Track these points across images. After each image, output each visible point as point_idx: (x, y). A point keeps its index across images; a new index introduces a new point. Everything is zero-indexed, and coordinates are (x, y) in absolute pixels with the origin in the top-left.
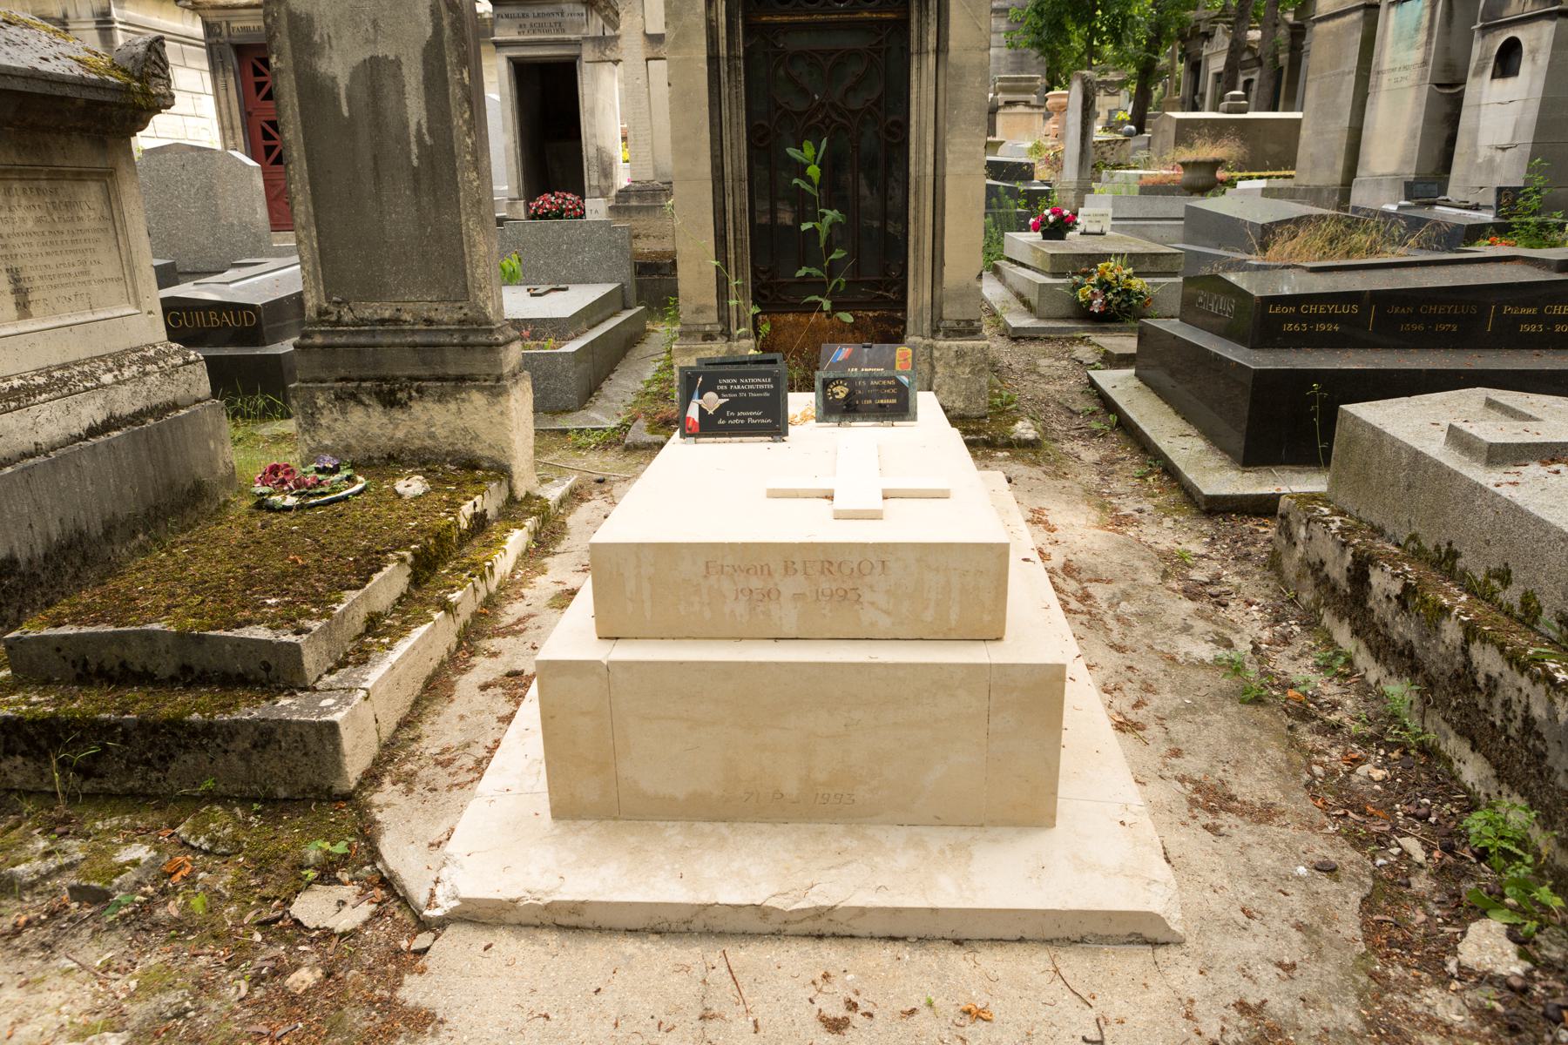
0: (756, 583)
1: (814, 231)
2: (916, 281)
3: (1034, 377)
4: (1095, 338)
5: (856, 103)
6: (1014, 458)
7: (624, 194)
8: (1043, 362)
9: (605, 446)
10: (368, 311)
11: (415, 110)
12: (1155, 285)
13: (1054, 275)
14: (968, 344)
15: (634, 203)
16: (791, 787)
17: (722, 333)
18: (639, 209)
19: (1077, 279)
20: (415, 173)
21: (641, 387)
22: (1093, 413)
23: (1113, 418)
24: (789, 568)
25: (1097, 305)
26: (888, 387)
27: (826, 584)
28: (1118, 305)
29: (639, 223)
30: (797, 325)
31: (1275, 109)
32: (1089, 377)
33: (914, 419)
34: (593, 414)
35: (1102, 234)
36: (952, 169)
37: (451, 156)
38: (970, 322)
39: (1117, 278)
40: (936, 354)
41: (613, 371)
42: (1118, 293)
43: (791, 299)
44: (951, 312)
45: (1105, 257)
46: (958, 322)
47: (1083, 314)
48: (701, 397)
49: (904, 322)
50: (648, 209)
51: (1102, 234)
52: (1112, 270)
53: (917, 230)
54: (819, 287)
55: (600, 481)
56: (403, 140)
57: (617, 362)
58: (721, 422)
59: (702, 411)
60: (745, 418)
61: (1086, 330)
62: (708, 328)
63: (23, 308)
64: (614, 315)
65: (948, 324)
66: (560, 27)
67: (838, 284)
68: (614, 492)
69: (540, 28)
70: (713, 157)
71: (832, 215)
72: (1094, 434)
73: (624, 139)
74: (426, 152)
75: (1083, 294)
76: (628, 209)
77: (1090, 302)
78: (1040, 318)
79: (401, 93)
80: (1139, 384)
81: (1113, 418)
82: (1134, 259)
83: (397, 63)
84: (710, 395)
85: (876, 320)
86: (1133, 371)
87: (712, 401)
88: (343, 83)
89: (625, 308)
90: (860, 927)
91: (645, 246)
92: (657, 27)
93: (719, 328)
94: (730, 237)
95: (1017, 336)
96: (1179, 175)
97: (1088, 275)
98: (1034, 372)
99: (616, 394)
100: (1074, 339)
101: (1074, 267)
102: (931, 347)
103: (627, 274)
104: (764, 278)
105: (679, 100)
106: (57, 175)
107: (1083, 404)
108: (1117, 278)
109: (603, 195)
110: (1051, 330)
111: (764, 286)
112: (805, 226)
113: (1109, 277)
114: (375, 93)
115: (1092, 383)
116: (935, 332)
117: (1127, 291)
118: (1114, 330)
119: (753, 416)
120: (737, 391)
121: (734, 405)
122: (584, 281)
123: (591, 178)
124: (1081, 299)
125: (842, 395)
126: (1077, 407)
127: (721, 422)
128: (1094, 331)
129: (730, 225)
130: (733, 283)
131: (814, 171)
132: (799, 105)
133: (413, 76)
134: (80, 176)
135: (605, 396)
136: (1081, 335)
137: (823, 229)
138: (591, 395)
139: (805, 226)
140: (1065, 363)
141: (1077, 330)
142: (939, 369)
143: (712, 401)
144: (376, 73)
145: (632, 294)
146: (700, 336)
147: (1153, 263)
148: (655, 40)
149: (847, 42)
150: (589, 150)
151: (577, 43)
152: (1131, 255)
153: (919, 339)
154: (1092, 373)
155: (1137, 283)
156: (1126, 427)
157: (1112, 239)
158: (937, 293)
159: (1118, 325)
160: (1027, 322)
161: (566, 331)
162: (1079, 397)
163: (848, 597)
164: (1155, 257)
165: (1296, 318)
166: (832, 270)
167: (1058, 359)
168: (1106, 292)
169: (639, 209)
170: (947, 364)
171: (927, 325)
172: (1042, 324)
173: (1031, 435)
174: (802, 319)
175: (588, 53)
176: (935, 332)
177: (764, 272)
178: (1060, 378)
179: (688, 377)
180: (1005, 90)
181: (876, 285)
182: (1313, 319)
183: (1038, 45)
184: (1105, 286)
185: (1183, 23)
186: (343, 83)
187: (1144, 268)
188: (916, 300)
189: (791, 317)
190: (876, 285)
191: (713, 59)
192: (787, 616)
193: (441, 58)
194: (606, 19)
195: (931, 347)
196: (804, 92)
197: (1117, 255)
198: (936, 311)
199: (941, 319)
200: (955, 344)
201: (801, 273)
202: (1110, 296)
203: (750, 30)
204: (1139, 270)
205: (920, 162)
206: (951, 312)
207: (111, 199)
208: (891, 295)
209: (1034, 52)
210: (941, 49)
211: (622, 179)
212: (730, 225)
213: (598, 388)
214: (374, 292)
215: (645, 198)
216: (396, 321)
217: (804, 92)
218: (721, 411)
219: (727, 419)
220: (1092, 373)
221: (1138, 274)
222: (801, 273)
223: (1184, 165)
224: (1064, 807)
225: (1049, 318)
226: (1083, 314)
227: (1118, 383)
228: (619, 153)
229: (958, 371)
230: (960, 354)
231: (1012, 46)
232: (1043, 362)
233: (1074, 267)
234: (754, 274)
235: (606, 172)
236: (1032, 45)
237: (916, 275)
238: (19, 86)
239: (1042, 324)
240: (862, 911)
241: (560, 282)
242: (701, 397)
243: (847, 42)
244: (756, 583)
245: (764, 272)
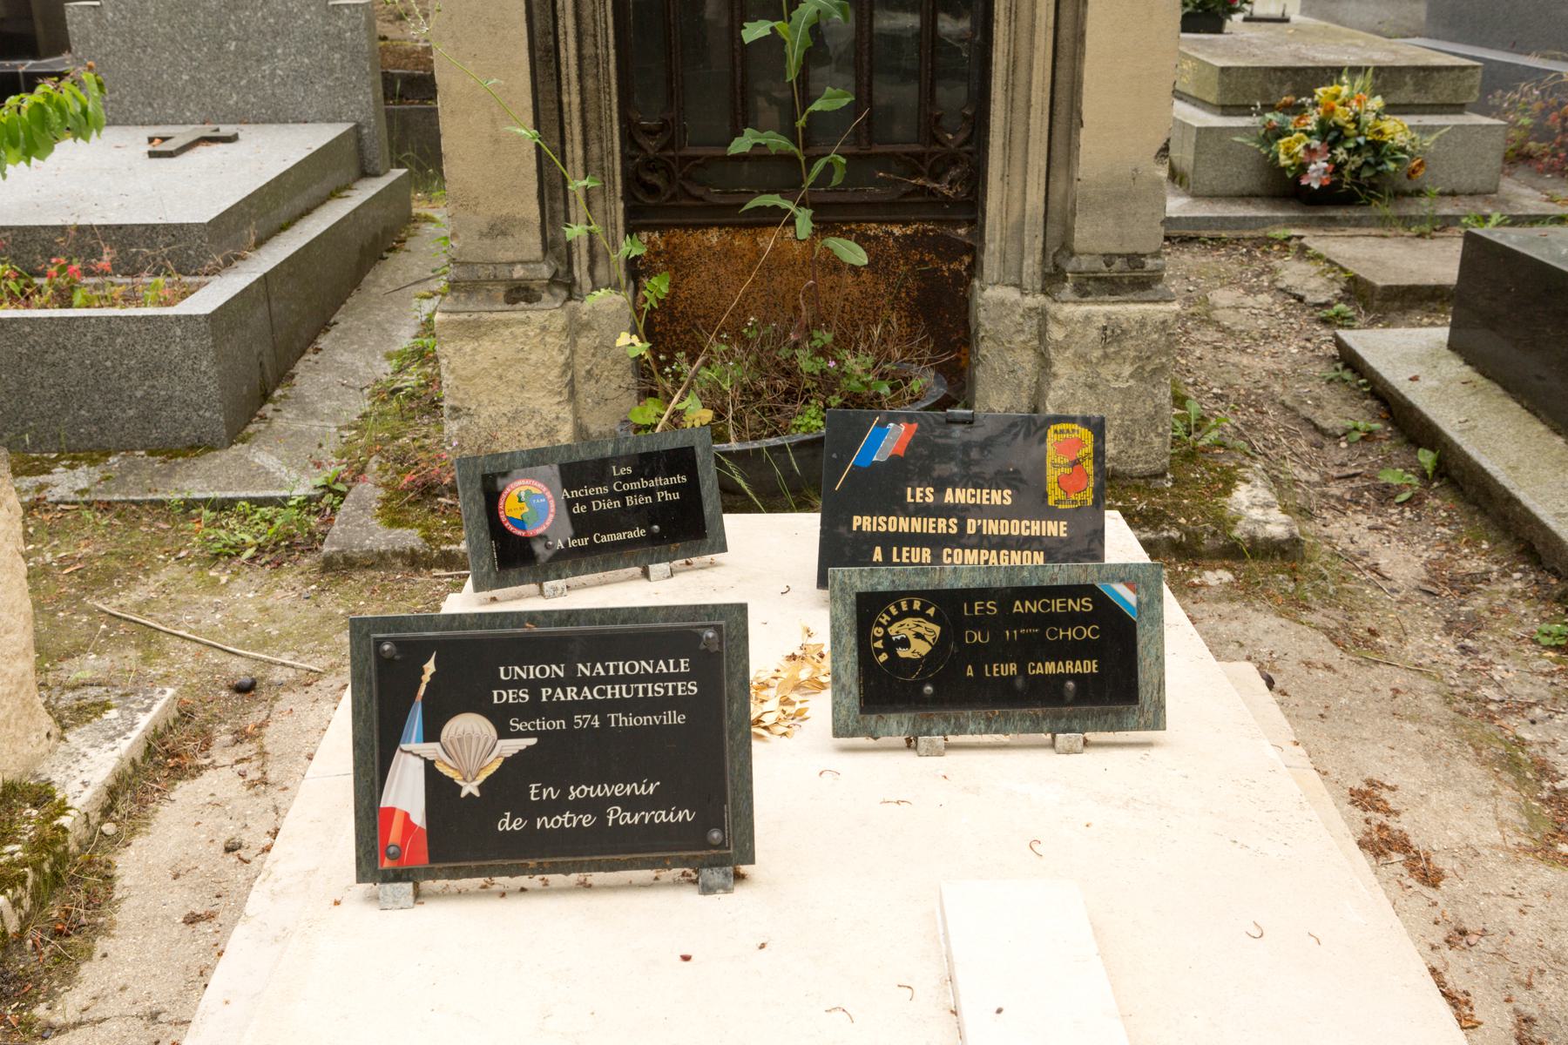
1: (773, 42)
2: (1008, 160)
3: (1211, 334)
4: (1316, 241)
6: (1246, 590)
8: (1223, 297)
9: (280, 551)
12: (1426, 130)
13: (1226, 110)
14: (1129, 310)
17: (553, 281)
19: (1274, 118)
21: (384, 369)
22: (1369, 436)
23: (1426, 458)
25: (1316, 174)
26: (1071, 619)
28: (1356, 173)
30: (728, 253)
32: (1339, 344)
33: (1157, 721)
34: (263, 457)
35: (1284, 20)
38: (1134, 259)
39: (1356, 120)
40: (1056, 333)
41: (325, 326)
42: (1357, 149)
43: (714, 196)
44: (1094, 236)
45: (1330, 74)
46: (1109, 258)
47: (1285, 188)
48: (432, 733)
49: (973, 250)
51: (1284, 20)
52: (1348, 100)
53: (1013, 39)
54: (780, 171)
55: (245, 689)
57: (338, 301)
58: (509, 824)
59: (438, 786)
60: (597, 806)
61: (1290, 222)
62: (519, 272)
64: (335, 193)
65: (1085, 264)
67: (829, 168)
68: (271, 734)
70: (1079, 37)
72: (1386, 495)
75: (1288, 150)
77: (1303, 168)
78: (1195, 196)
80: (1467, 371)
81: (1426, 458)
82: (1386, 78)
84: (468, 727)
85: (908, 243)
86: (1442, 333)
87: (474, 747)
89: (365, 173)
93: (545, 271)
94: (569, 52)
98: (1207, 321)
99: (326, 394)
100: (1269, 241)
101: (1266, 94)
102: (1043, 314)
103: (365, 100)
104: (651, 145)
107: (1343, 413)
108: (1356, 120)
110: (1224, 222)
111: (651, 165)
112: (754, 31)
113: (1342, 116)
115: (1350, 360)
116: (1052, 278)
117: (1376, 146)
118: (1347, 222)
119: (623, 799)
120: (565, 710)
122: (276, 114)
124: (1284, 161)
125: (920, 648)
126: (1331, 422)
127: (509, 824)
128: (1305, 224)
129: (568, 22)
130: (577, 184)
135: (300, 400)
136: (1281, 233)
138: (265, 397)
139: (754, 31)
140: (1265, 299)
141: (1274, 222)
142: (1062, 368)
145: (378, 143)
146: (500, 291)
147: (1420, 87)
152: (1379, 70)
153: (1012, 294)
154: (1346, 335)
155: (1397, 129)
156: (1459, 478)
157: (1300, 31)
158: (1059, 186)
159: (1355, 213)
161: (203, 255)
162: (1324, 391)
164: (1425, 74)
166: (815, 134)
167: (1250, 291)
168: (1333, 145)
170: (1082, 358)
171: (1032, 265)
172: (1203, 210)
173: (1277, 525)
174: (741, 241)
176: (1052, 278)
177: (650, 133)
178: (1265, 336)
179: (383, 663)
181: (913, 164)
184: (1331, 134)
187: (1402, 97)
188: (1006, 204)
189: (713, 237)
190: (913, 164)
195: (1043, 314)
197: (1355, 70)
198: (1055, 231)
199: (1067, 248)
200: (1101, 310)
201: (742, 145)
202: (1341, 154)
204: (1393, 99)
206: (1094, 236)
208: (943, 188)
212: (568, 22)
213: (284, 375)
218: (507, 783)
219: (530, 811)
220: (1346, 335)
221: (1392, 109)
222: (742, 145)
225: (1213, 197)
226: (1285, 188)
227: (1412, 355)
229: (1106, 372)
230: (1112, 335)
232: (1223, 297)
233: (1266, 94)
234: (628, 138)
237: (1008, 144)
239: (1203, 210)
241: (225, 120)
242: (432, 733)
245: (650, 133)
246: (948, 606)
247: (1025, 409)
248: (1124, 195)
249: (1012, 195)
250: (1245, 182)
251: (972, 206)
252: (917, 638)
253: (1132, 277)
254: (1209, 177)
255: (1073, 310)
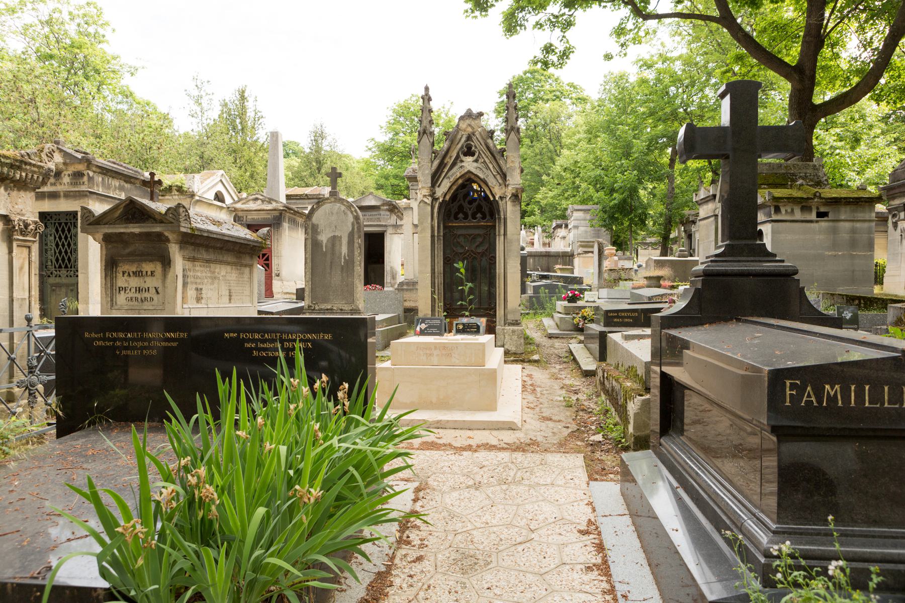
0: (428, 352)
5: (480, 250)
7: (401, 284)
10: (323, 306)
11: (344, 250)
13: (566, 314)
14: (516, 328)
15: (405, 287)
16: (434, 400)
18: (407, 290)
20: (342, 267)
24: (436, 348)
27: (444, 352)
29: (407, 295)
31: (666, 256)
36: (509, 271)
37: (353, 262)
44: (510, 317)
50: (411, 290)
56: (340, 257)
63: (230, 302)
66: (379, 220)
69: (371, 220)
71: (470, 285)
73: (402, 265)
74: (346, 261)
76: (403, 290)
79: (341, 245)
83: (341, 237)
87: (423, 326)
88: (325, 242)
90: (448, 425)
91: (408, 304)
92: (416, 222)
95: (551, 336)
96: (646, 282)
97: (577, 314)
103: (400, 311)
105: (422, 249)
106: (242, 265)
109: (392, 286)
113: (585, 314)
114: (333, 245)
119: (434, 330)
121: (430, 327)
122: (384, 313)
123: (388, 279)
131: (463, 270)
132: (462, 251)
133: (345, 241)
134: (246, 266)
137: (467, 289)
143: (423, 326)
144: (334, 240)
145: (402, 319)
148: (416, 226)
149: (477, 232)
150: (387, 267)
151: (386, 226)
160: (557, 331)
163: (449, 355)
165: (618, 317)
169: (407, 290)
175: (390, 231)
180: (582, 246)
181: (486, 309)
182: (622, 317)
183: (605, 226)
185: (682, 216)
186: (325, 242)
190: (486, 309)
191: (433, 236)
192: (435, 360)
193: (353, 236)
194: (398, 216)
196: (462, 246)
200: (512, 328)
203: (445, 227)
205: (499, 269)
206: (510, 317)
207: (251, 272)
209: (604, 229)
210: (505, 234)
211: (400, 279)
214: (325, 300)
215: (410, 286)
216: (331, 309)
217: (462, 246)
218: (426, 329)
223: (646, 278)
224: (498, 408)
228: (399, 270)
230: (513, 331)
231: (592, 226)
235: (394, 277)
236: (602, 226)
238: (242, 241)
240: (448, 421)
243: (477, 232)
244: (428, 352)
246: (463, 324)
247: (568, 413)
248: (514, 311)
249: (500, 312)
250: (570, 328)
251: (495, 315)
252: (461, 327)
253: (517, 323)
254: (563, 327)
255: (507, 328)
